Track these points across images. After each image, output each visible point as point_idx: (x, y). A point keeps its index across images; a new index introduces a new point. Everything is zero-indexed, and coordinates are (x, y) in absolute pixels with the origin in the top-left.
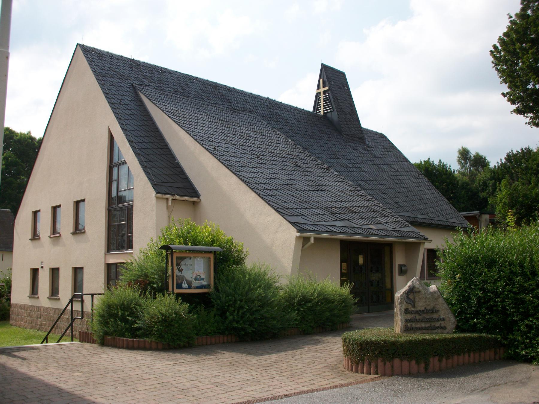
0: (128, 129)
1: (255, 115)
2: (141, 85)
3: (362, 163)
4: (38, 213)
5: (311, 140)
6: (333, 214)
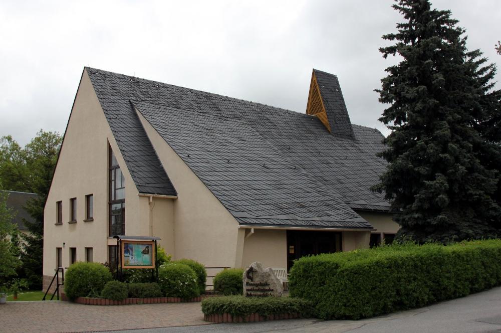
0: (121, 140)
1: (243, 121)
2: (138, 101)
3: (346, 159)
4: (91, 197)
5: (296, 141)
6: (281, 209)
